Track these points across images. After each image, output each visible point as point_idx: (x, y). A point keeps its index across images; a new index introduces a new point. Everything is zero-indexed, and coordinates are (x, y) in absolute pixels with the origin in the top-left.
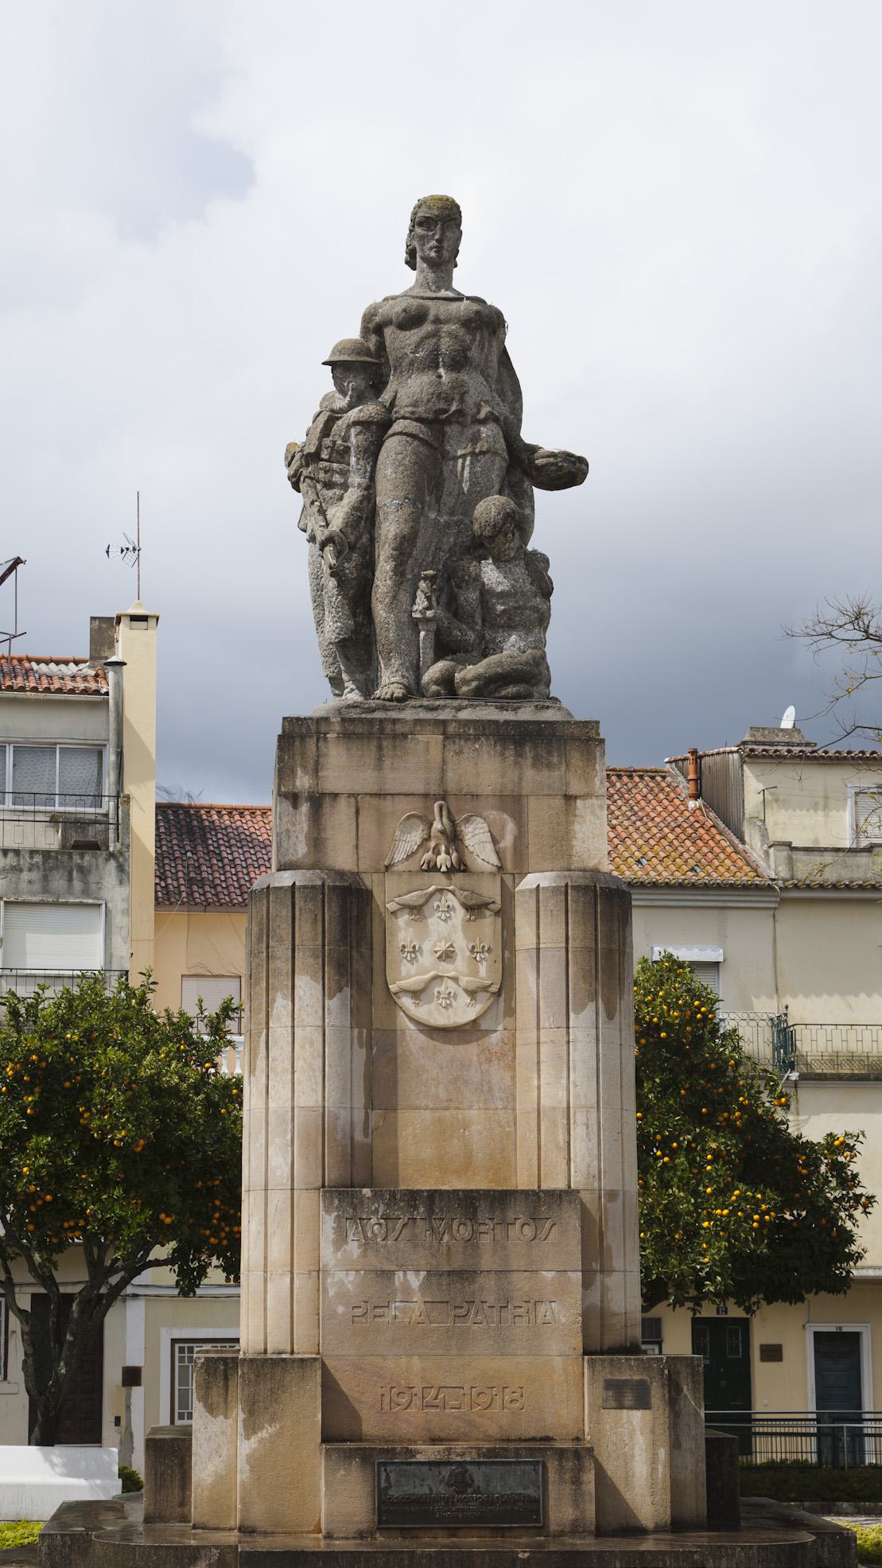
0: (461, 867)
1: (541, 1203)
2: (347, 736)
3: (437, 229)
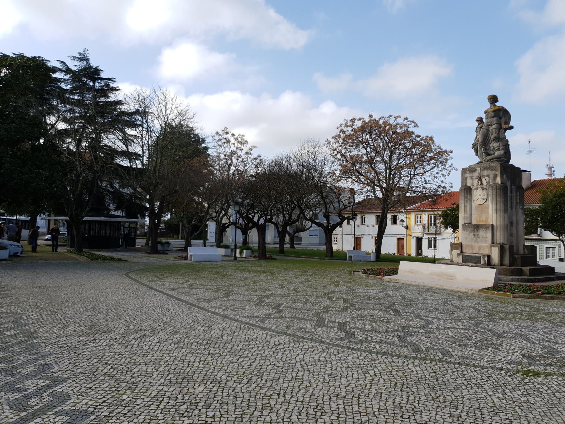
0: (482, 184)
3: (493, 99)
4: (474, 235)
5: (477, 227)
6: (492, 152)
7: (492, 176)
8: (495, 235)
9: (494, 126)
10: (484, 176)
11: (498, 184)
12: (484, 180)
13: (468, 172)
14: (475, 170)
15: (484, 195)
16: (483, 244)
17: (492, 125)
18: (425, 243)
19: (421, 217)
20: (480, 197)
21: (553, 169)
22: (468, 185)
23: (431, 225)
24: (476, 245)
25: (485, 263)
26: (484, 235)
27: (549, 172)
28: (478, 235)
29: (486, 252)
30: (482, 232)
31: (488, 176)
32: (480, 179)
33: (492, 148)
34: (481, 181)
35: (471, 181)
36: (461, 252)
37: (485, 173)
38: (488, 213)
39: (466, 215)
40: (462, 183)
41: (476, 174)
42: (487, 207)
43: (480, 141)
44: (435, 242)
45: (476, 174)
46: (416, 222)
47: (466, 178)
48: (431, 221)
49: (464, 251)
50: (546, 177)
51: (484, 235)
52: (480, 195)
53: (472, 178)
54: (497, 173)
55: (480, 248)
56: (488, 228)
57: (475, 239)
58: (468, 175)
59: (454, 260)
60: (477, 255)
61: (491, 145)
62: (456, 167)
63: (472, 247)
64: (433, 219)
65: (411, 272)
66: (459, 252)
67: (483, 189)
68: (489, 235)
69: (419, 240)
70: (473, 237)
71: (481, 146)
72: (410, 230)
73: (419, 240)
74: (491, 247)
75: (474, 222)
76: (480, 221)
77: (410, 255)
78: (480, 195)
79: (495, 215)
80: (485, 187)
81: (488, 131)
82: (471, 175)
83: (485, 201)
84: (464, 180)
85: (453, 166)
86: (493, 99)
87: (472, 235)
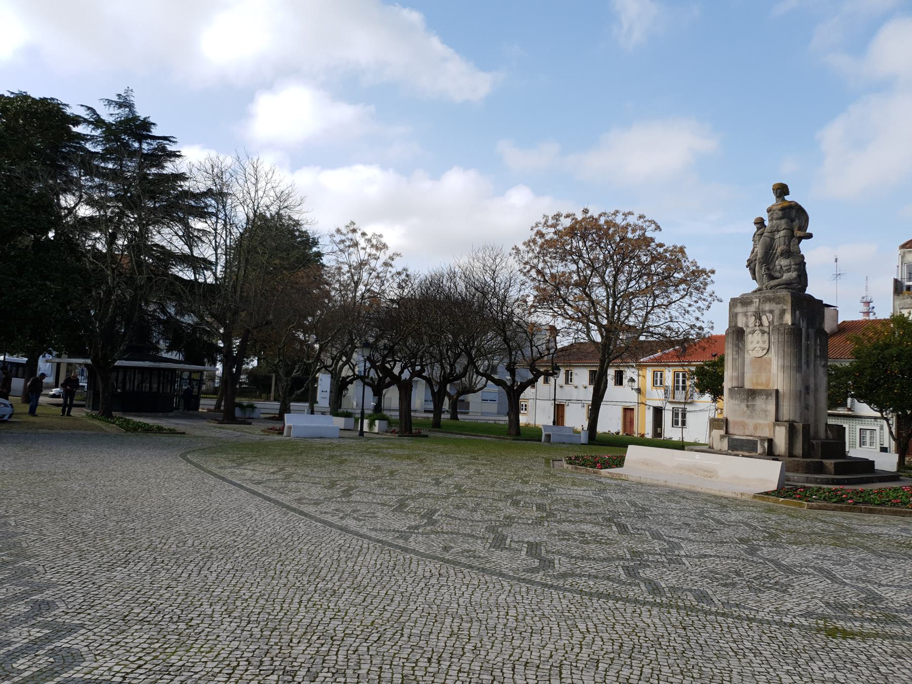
0: (761, 325)
1: (766, 393)
2: (741, 303)
3: (781, 190)
4: (748, 406)
5: (752, 394)
6: (778, 274)
7: (777, 313)
8: (781, 407)
9: (782, 233)
10: (764, 312)
11: (786, 324)
12: (764, 318)
13: (739, 305)
14: (751, 302)
15: (764, 342)
16: (761, 421)
17: (778, 231)
18: (667, 417)
19: (661, 375)
20: (758, 345)
21: (871, 305)
22: (740, 325)
23: (678, 388)
24: (751, 423)
25: (764, 452)
26: (764, 406)
27: (865, 309)
28: (754, 406)
29: (767, 434)
30: (759, 402)
31: (771, 312)
32: (758, 316)
33: (778, 267)
34: (760, 319)
35: (744, 319)
36: (727, 432)
37: (767, 307)
38: (770, 372)
39: (735, 374)
40: (730, 321)
41: (752, 309)
42: (769, 362)
43: (759, 256)
44: (684, 416)
45: (752, 309)
46: (655, 383)
47: (736, 314)
48: (678, 382)
49: (731, 431)
50: (860, 317)
51: (764, 406)
52: (758, 342)
53: (745, 314)
54: (785, 307)
55: (756, 427)
56: (771, 395)
57: (748, 412)
58: (739, 309)
59: (715, 446)
60: (751, 438)
61: (777, 263)
62: (719, 297)
63: (744, 425)
64: (681, 379)
65: (646, 463)
66: (722, 432)
67: (763, 332)
68: (772, 407)
69: (658, 412)
70: (745, 409)
71: (761, 263)
72: (644, 396)
73: (658, 412)
74: (774, 425)
75: (748, 385)
76: (757, 384)
77: (643, 435)
78: (758, 342)
79: (781, 374)
80: (767, 329)
81: (772, 239)
82: (744, 309)
83: (765, 351)
84: (733, 317)
85: (716, 294)
86: (781, 190)
87: (743, 405)
